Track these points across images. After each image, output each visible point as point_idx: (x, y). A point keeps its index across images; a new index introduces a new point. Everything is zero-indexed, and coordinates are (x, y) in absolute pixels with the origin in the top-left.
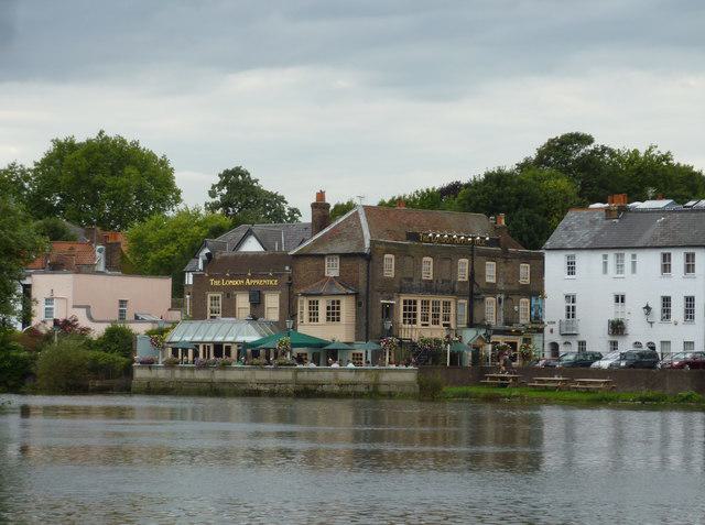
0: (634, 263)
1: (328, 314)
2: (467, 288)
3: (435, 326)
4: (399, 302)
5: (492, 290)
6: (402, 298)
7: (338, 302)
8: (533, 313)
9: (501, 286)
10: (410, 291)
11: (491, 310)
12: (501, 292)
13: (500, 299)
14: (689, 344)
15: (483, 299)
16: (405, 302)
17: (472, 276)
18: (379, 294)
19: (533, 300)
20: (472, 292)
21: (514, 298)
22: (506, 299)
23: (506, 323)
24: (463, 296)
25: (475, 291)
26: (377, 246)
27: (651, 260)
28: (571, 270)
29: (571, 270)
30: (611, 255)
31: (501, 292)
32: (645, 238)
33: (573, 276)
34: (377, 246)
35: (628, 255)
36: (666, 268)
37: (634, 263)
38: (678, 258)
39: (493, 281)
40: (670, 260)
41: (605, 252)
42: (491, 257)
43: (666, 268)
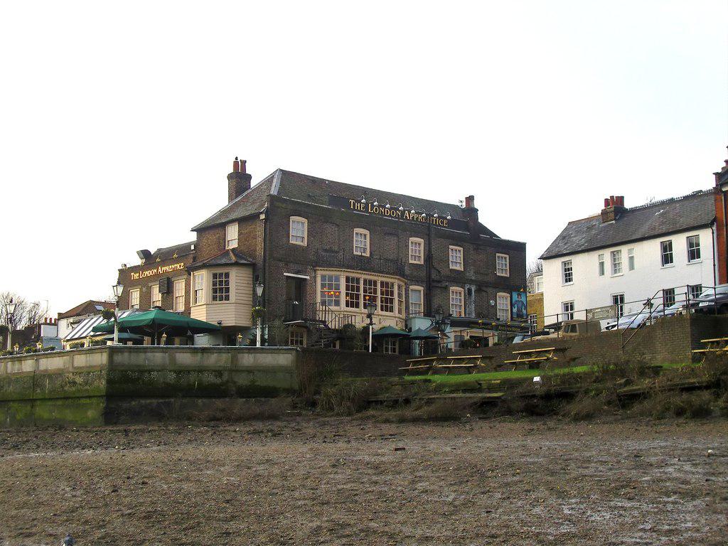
0: (631, 259)
1: (214, 284)
2: (423, 274)
3: (384, 313)
4: (315, 277)
5: (458, 278)
6: (319, 273)
7: (227, 275)
8: (515, 310)
9: (471, 275)
10: (329, 265)
11: (457, 301)
12: (471, 282)
13: (470, 291)
14: (696, 289)
15: (446, 288)
16: (323, 278)
17: (429, 258)
18: (281, 264)
19: (515, 296)
20: (429, 276)
21: (490, 290)
22: (479, 290)
23: (479, 315)
24: (417, 282)
25: (433, 276)
26: (278, 204)
27: (652, 249)
28: (568, 277)
29: (568, 277)
30: (607, 254)
31: (471, 282)
32: (644, 230)
33: (571, 283)
34: (278, 204)
35: (624, 250)
36: (667, 258)
37: (631, 259)
38: (679, 243)
39: (460, 268)
40: (671, 250)
41: (601, 252)
42: (458, 241)
43: (667, 258)
